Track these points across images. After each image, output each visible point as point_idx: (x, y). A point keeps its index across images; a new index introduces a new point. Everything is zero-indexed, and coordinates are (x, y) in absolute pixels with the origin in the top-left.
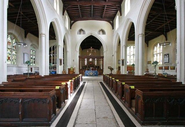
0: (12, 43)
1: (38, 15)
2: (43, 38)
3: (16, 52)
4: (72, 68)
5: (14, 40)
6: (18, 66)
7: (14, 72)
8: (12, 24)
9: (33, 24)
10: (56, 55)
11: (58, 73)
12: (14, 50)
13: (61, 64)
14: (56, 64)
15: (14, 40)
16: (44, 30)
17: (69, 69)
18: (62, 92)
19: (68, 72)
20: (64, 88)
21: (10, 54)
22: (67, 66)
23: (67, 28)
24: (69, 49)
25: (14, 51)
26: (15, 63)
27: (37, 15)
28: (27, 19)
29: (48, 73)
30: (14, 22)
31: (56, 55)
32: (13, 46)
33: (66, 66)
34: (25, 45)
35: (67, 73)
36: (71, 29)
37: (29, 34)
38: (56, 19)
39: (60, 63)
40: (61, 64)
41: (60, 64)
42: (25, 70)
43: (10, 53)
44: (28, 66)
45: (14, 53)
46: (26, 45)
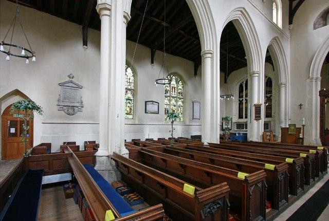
0: (177, 88)
1: (245, 39)
2: (256, 80)
3: (183, 102)
4: (292, 128)
5: (180, 83)
6: (184, 123)
7: (153, 132)
8: (136, 46)
9: (234, 59)
10: (246, 100)
11: (250, 139)
12: (180, 99)
13: (258, 117)
14: (246, 117)
15: (180, 83)
16: (211, 44)
17: (284, 130)
18: (281, 177)
19: (282, 136)
20: (287, 170)
21: (175, 106)
22: (280, 122)
23: (280, 25)
24: (286, 75)
25: (166, 99)
26: (182, 118)
27: (243, 36)
28: (192, 40)
29: (216, 140)
30: (135, 41)
31: (246, 100)
32: (179, 93)
33: (277, 121)
34: (28, 58)
35: (279, 140)
36: (291, 22)
37: (158, 52)
38: (243, 11)
39: (256, 114)
40: (258, 117)
41: (256, 117)
42: (179, 132)
43: (175, 103)
44: (172, 122)
45: (180, 103)
46: (34, 59)
